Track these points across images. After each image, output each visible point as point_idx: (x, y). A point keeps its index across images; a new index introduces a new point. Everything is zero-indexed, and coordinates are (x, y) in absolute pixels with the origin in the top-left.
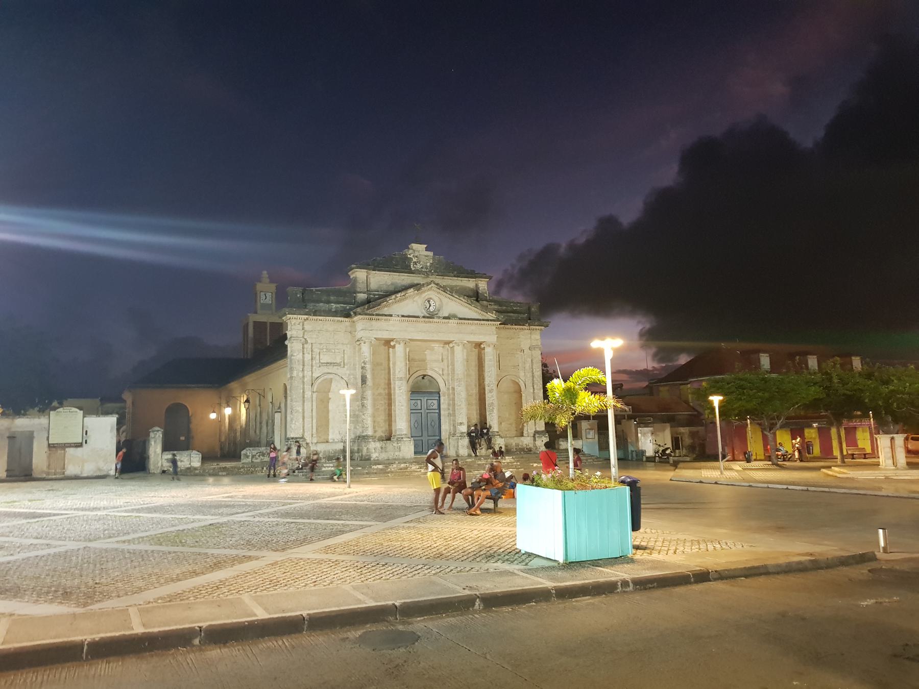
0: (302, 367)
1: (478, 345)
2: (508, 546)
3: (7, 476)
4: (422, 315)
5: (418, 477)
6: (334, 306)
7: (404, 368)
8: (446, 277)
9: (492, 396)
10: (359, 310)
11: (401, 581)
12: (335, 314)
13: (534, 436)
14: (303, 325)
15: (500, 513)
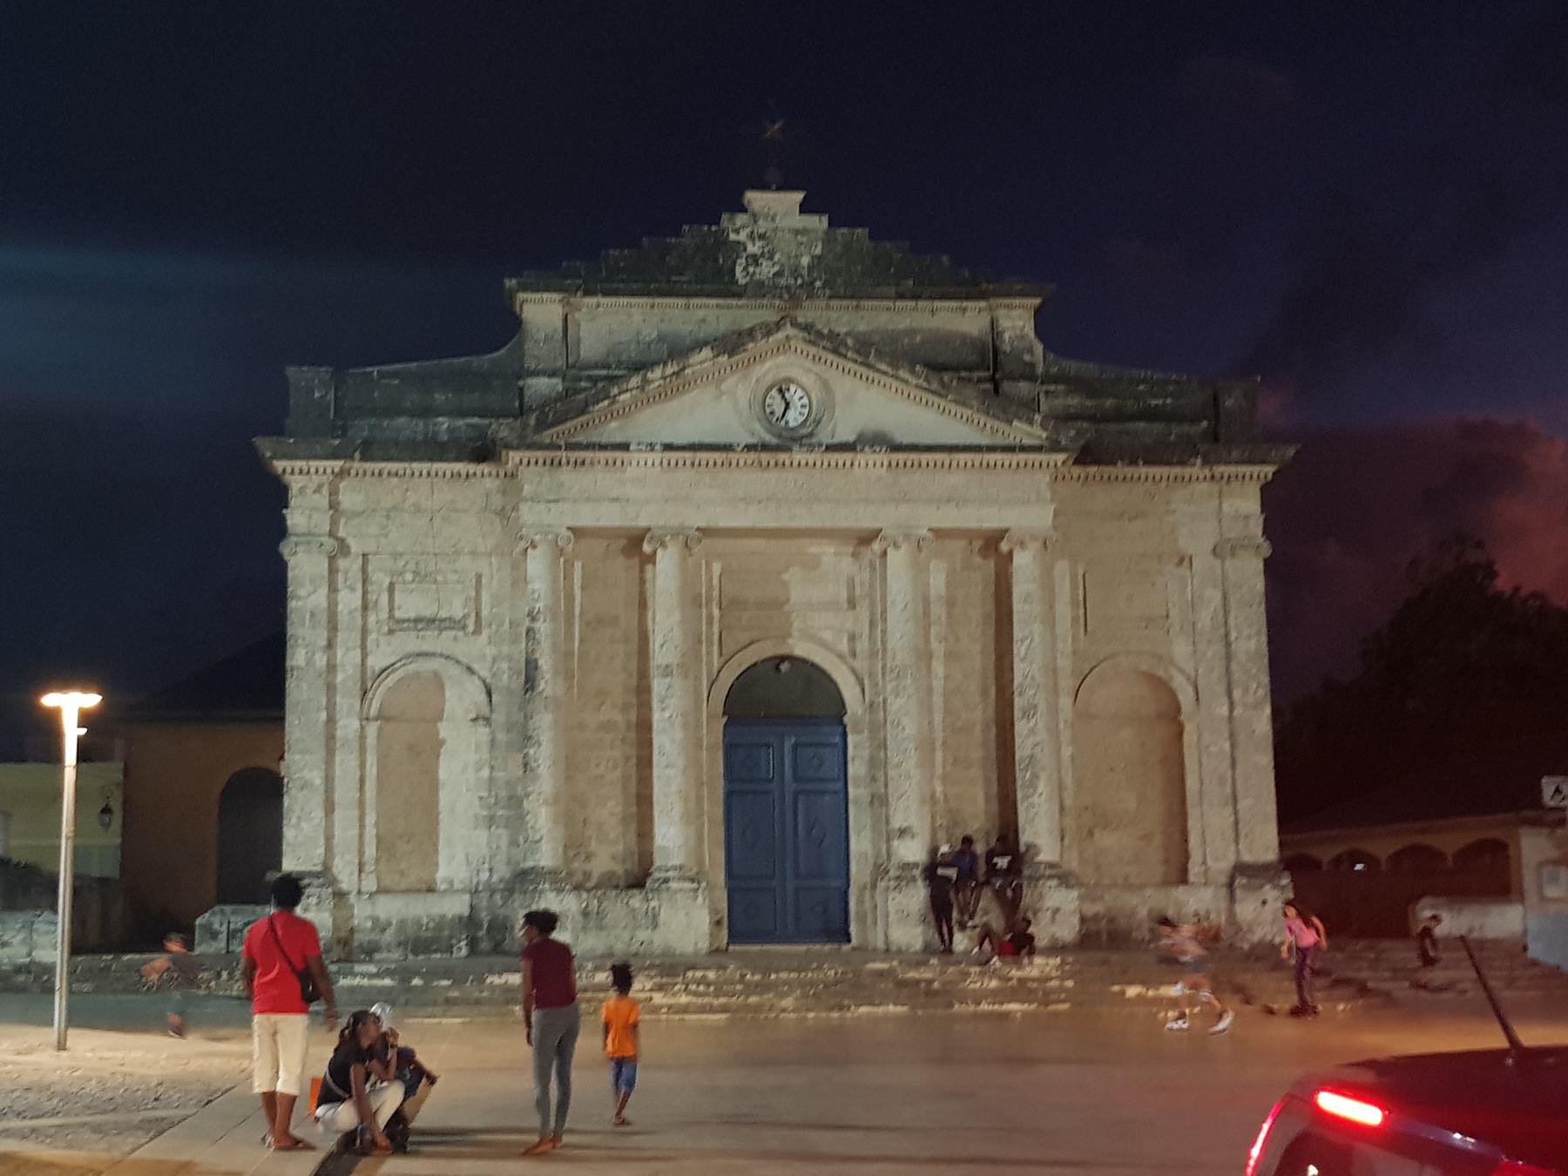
0: (325, 634)
1: (992, 544)
6: (444, 423)
12: (434, 450)
13: (1230, 885)
14: (334, 493)
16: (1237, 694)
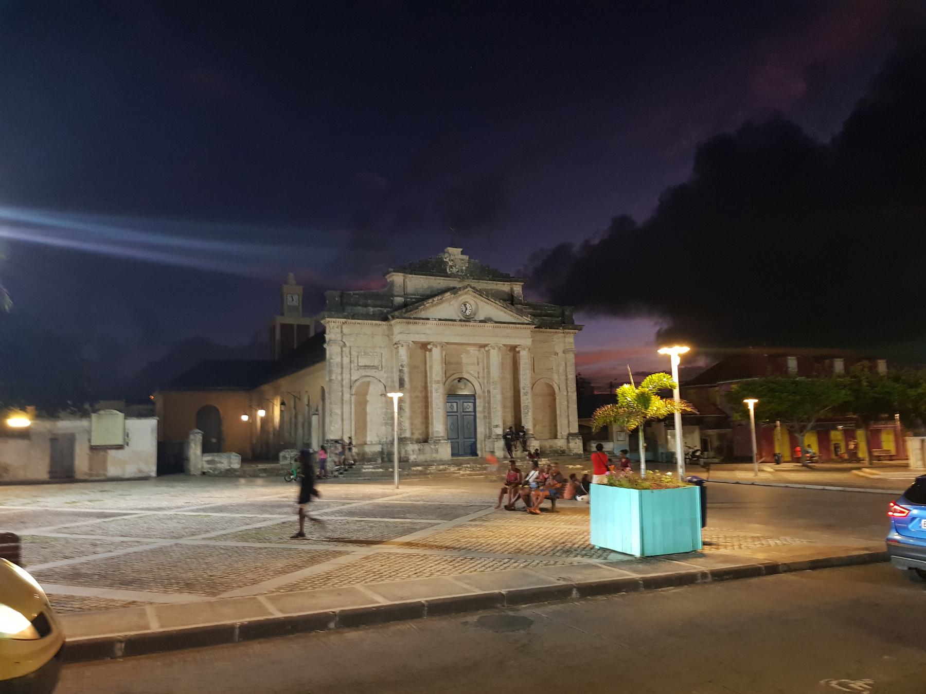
0: (340, 370)
1: (513, 349)
2: (581, 543)
3: (50, 478)
4: (459, 319)
5: (457, 478)
6: (371, 309)
7: (440, 371)
8: (438, 278)
9: (527, 399)
10: (396, 313)
11: (495, 573)
12: (373, 317)
13: (568, 439)
14: (342, 328)
15: (558, 512)
16: (569, 389)
